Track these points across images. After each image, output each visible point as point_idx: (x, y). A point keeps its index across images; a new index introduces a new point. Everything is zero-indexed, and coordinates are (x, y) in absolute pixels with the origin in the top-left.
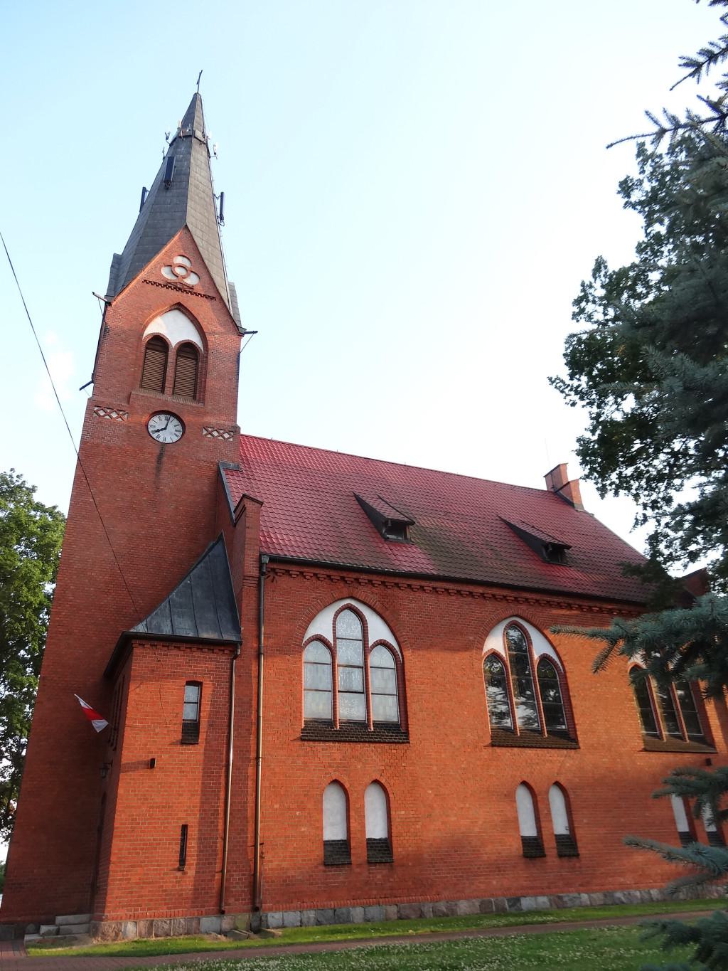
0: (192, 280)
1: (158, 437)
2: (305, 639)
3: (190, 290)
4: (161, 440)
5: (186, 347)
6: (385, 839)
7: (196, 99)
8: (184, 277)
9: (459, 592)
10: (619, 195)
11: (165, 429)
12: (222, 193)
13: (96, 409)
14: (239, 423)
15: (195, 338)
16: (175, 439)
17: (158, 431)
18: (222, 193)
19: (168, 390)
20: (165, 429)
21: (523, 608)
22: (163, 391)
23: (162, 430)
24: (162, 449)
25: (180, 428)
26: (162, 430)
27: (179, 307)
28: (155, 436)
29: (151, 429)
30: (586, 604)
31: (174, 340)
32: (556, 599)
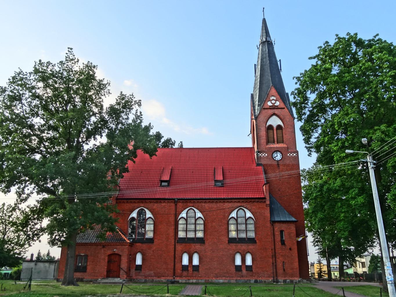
0: (278, 103)
1: (276, 159)
2: (229, 218)
4: (277, 160)
5: (279, 127)
6: (152, 239)
7: (264, 21)
8: (275, 103)
9: (131, 202)
10: (163, 136)
14: (298, 149)
15: (281, 124)
16: (280, 158)
17: (276, 157)
19: (276, 142)
21: (243, 204)
24: (278, 163)
25: (281, 155)
28: (275, 159)
29: (273, 157)
30: (143, 201)
32: (152, 201)
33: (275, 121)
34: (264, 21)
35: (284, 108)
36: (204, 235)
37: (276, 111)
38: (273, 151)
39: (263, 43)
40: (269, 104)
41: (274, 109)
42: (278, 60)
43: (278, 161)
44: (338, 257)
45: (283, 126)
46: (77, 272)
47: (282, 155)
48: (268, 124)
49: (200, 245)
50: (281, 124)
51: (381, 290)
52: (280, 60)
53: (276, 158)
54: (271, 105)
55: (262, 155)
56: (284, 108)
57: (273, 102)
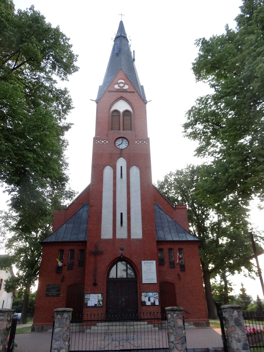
0: (126, 87)
1: (119, 147)
3: (125, 91)
4: (120, 148)
5: (126, 112)
7: (121, 23)
8: (123, 87)
11: (122, 144)
12: (134, 51)
13: (96, 140)
15: (129, 109)
17: (119, 145)
18: (134, 51)
20: (122, 144)
22: (119, 130)
23: (121, 144)
25: (127, 142)
26: (121, 144)
27: (121, 98)
28: (118, 147)
29: (116, 145)
31: (121, 110)
33: (122, 106)
34: (121, 23)
35: (134, 92)
36: (92, 307)
37: (124, 95)
38: (115, 139)
39: (117, 38)
40: (116, 87)
41: (122, 92)
42: (132, 52)
43: (122, 150)
44: (16, 13)
45: (132, 112)
46: (116, 321)
47: (129, 144)
48: (113, 108)
49: (163, 229)
50: (129, 109)
51: (184, 328)
52: (134, 51)
53: (120, 146)
54: (118, 88)
55: (101, 142)
56: (134, 92)
57: (122, 85)
